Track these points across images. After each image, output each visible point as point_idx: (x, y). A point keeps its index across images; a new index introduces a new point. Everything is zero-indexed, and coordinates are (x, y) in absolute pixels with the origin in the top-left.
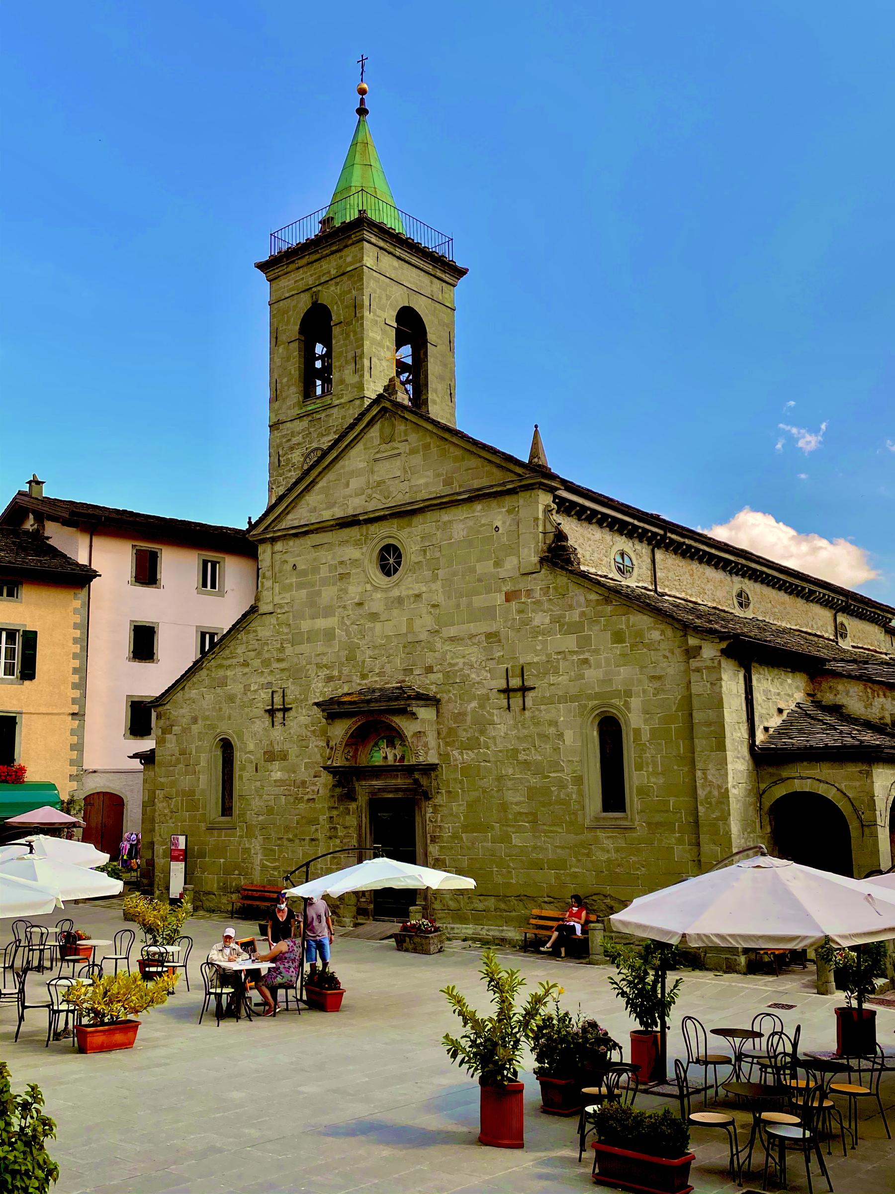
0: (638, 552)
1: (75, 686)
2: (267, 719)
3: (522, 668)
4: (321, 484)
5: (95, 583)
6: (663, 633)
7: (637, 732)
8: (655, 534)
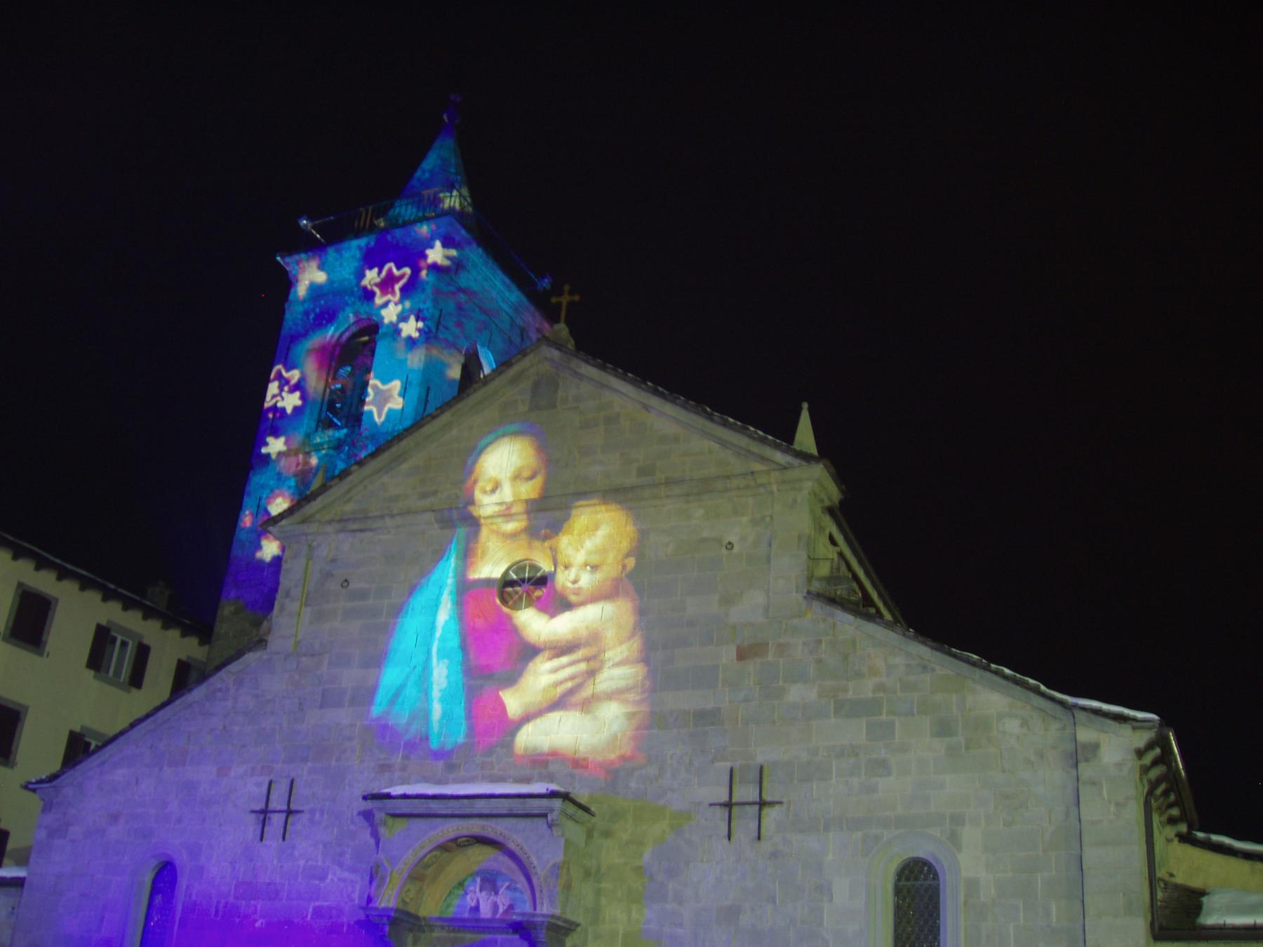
3: (761, 768)
6: (1024, 723)
7: (973, 885)
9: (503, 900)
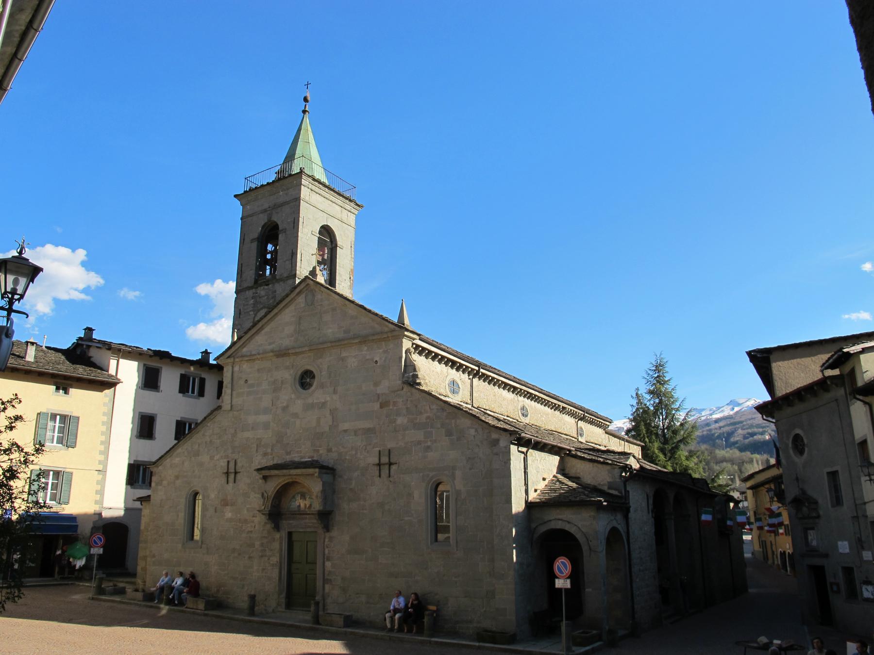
0: (462, 378)
1: (101, 453)
2: (223, 479)
4: (267, 329)
5: (118, 386)
6: (476, 431)
8: (473, 370)
9: (308, 503)
